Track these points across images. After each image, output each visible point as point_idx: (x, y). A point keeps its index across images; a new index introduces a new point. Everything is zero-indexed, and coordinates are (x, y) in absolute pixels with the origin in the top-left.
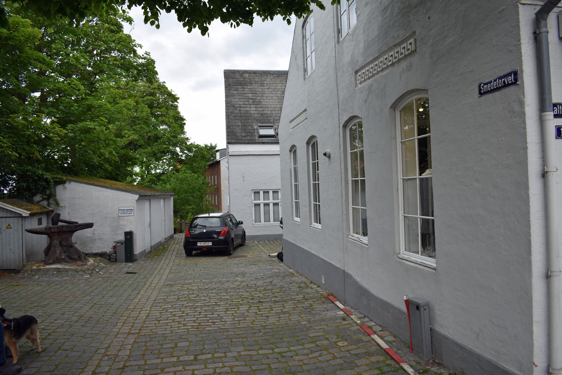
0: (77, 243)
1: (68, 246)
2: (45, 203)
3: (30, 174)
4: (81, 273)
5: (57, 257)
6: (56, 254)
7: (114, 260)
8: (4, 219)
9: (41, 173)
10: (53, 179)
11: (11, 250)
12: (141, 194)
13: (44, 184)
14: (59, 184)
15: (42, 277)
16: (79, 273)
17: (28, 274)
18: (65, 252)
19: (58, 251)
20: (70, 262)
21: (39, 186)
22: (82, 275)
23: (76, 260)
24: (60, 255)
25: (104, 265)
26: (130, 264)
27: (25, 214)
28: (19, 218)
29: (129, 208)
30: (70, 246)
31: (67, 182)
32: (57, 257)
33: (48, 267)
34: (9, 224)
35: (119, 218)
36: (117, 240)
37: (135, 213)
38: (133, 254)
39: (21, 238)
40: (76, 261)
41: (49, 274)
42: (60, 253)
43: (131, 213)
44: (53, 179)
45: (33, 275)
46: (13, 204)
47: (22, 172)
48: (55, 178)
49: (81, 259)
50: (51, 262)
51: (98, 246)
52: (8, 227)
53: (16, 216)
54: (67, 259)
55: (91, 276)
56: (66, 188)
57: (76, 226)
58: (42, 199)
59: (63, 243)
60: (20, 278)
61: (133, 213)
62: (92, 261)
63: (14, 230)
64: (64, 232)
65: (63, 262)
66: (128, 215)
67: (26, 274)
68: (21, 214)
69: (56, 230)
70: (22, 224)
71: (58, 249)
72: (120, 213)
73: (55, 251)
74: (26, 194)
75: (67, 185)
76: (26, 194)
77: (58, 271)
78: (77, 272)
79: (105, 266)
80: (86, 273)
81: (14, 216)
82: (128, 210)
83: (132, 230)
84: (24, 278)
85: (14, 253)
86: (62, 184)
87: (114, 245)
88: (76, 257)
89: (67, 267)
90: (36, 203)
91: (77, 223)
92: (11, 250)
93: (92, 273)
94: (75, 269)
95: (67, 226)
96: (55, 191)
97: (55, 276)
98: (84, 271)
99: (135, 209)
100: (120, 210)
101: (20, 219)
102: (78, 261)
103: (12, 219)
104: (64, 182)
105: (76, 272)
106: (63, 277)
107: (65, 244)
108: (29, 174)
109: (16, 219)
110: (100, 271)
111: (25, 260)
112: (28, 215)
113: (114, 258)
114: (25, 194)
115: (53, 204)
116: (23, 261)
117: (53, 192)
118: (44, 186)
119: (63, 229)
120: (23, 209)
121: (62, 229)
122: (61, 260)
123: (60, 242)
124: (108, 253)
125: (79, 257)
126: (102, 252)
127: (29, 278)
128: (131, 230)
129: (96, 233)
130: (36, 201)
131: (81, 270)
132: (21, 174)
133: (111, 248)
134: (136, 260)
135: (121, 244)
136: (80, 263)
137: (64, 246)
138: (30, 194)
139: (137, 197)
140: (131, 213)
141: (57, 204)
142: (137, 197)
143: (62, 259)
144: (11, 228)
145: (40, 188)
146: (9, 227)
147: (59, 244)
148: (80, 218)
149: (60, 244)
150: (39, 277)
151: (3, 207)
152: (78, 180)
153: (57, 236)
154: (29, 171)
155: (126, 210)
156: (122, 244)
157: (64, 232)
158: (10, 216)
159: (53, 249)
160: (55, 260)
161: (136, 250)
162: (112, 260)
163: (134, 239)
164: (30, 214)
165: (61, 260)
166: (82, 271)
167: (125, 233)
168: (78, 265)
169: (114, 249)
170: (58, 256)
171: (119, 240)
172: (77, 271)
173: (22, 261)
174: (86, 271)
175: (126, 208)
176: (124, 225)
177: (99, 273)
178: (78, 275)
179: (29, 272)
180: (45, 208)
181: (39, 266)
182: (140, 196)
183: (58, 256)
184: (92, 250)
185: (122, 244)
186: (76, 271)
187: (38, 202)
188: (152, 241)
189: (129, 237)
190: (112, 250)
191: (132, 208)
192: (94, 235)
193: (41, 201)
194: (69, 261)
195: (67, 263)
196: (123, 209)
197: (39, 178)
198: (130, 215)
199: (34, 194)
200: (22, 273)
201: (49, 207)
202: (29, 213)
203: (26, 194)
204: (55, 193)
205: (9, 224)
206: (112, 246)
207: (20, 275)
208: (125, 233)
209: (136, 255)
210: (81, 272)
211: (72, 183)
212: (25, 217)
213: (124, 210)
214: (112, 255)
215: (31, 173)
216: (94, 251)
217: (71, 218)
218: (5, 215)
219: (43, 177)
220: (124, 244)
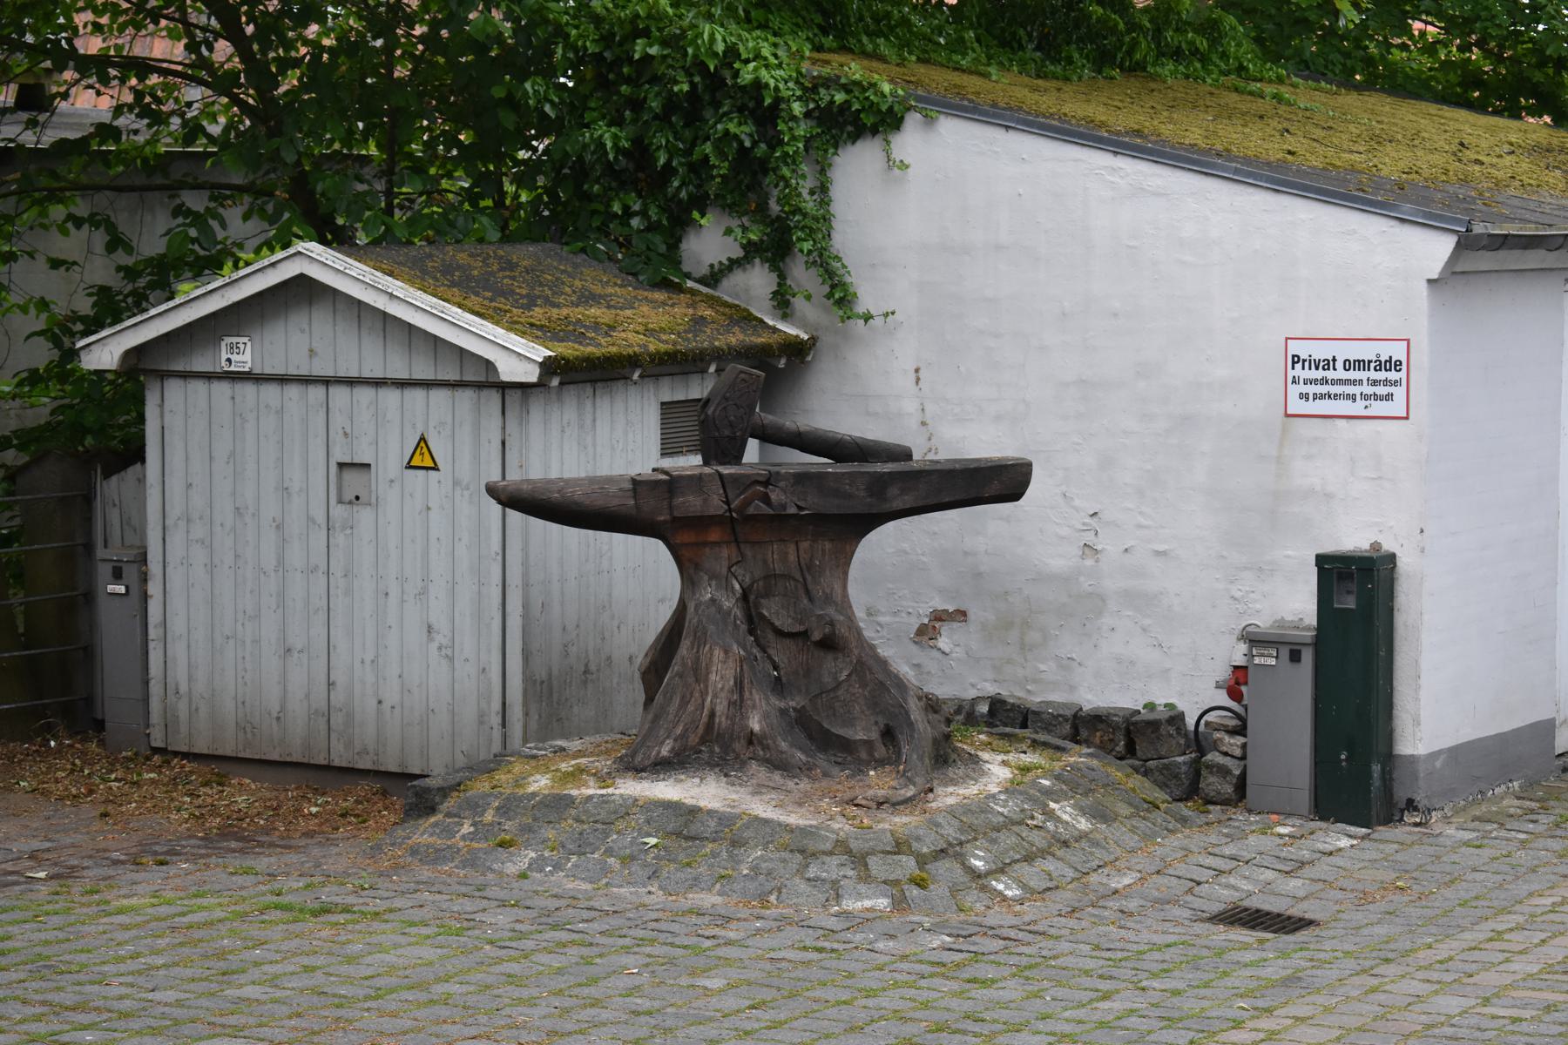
0: (971, 616)
1: (804, 635)
2: (756, 284)
3: (653, 51)
4: (832, 868)
5: (712, 715)
6: (704, 694)
7: (1229, 789)
8: (391, 396)
9: (720, 47)
10: (809, 89)
11: (430, 629)
12: (1478, 229)
13: (743, 130)
14: (855, 138)
15: (557, 867)
16: (812, 872)
17: (480, 831)
18: (779, 687)
19: (721, 674)
20: (806, 770)
21: (708, 148)
22: (835, 884)
23: (864, 755)
24: (739, 705)
25: (1083, 824)
26: (1340, 838)
27: (514, 360)
28: (485, 393)
29: (1366, 352)
30: (817, 636)
31: (912, 120)
32: (712, 715)
33: (631, 788)
34: (423, 439)
35: (1285, 430)
36: (1263, 622)
37: (1420, 395)
38: (1389, 757)
39: (496, 545)
40: (860, 768)
41: (609, 852)
42: (739, 685)
43: (1382, 390)
44: (809, 89)
45: (502, 845)
46: (421, 276)
47: (607, 40)
48: (828, 82)
49: (899, 753)
50: (665, 751)
51: (1119, 661)
52: (416, 462)
53: (468, 377)
54: (784, 745)
55: (900, 903)
56: (904, 166)
57: (879, 484)
58: (738, 253)
59: (774, 611)
60: (414, 851)
61: (1399, 392)
62: (1004, 774)
63: (456, 483)
64: (781, 524)
65: (754, 765)
66: (1357, 408)
67: (467, 828)
68: (489, 365)
69: (716, 505)
70: (503, 443)
71: (718, 654)
72: (1294, 391)
73: (699, 673)
74: (626, 208)
75: (911, 141)
76: (626, 208)
77: (678, 834)
78: (808, 855)
79: (1082, 836)
80: (866, 877)
81: (452, 375)
82: (1361, 364)
83: (1388, 546)
84: (435, 856)
85: (451, 659)
86: (874, 131)
87: (1240, 660)
88: (860, 732)
89: (762, 808)
90: (700, 281)
91: (906, 455)
92: (430, 629)
93: (920, 883)
94: (804, 832)
95: (803, 478)
96: (823, 189)
97: (645, 865)
98: (860, 860)
99: (1421, 358)
100: (1296, 359)
101: (494, 397)
102: (880, 763)
103: (439, 396)
104: (887, 122)
105: (799, 857)
106: (695, 884)
107: (784, 622)
108: (647, 58)
109: (466, 397)
110: (1001, 870)
111: (516, 713)
112: (531, 375)
113: (1224, 771)
114: (617, 208)
115: (808, 298)
116: (504, 725)
117: (809, 204)
118: (742, 150)
119: (775, 496)
120: (512, 326)
121: (766, 499)
122: (739, 746)
123: (745, 596)
124: (1190, 722)
125: (888, 735)
126: (1150, 706)
127: (471, 862)
128: (1376, 546)
129: (1109, 544)
130: (704, 270)
131: (842, 847)
132: (598, 57)
133: (1218, 686)
134: (1411, 805)
135: (1285, 652)
136: (879, 783)
137: (779, 633)
138: (653, 213)
139: (1436, 249)
140: (1382, 390)
141: (841, 297)
142: (1436, 249)
143: (751, 739)
144: (435, 468)
145: (713, 160)
146: (421, 459)
147: (738, 612)
148: (998, 418)
149: (750, 619)
150: (536, 865)
151: (381, 303)
152: (1030, 98)
153: (725, 552)
154: (646, 33)
155: (1349, 365)
156: (1295, 657)
157: (781, 524)
158: (428, 374)
159: (684, 650)
160: (693, 739)
161: (1417, 722)
162: (1213, 784)
163: (1402, 620)
164: (548, 367)
165: (739, 746)
166: (849, 852)
167: (1321, 560)
168: (852, 802)
169: (1235, 694)
170: (721, 708)
171: (1281, 623)
172: (812, 846)
173: (496, 720)
174: (873, 862)
175: (1345, 351)
176: (1329, 496)
177: (984, 888)
178: (803, 886)
179: (489, 817)
180: (747, 319)
181: (576, 775)
182: (1467, 244)
183: (721, 708)
184: (1072, 688)
185: (1295, 657)
186: (802, 846)
187: (714, 277)
188: (456, 685)
189: (1350, 603)
190: (1223, 699)
191: (1397, 352)
192: (1089, 562)
193: (734, 264)
194: (800, 756)
195: (777, 777)
196: (1321, 351)
197: (715, 82)
198: (1378, 408)
199: (679, 222)
200: (448, 815)
201: (785, 317)
202: (540, 353)
203: (628, 213)
204: (825, 202)
205: (423, 439)
206: (1223, 673)
207: (423, 833)
208: (1321, 560)
209: (1412, 760)
210: (834, 861)
211: (952, 130)
212: (522, 387)
213: (1330, 364)
214: (1215, 746)
215: (664, 43)
216: (1094, 696)
217: (929, 408)
218: (423, 371)
219: (736, 74)
220: (1307, 656)
